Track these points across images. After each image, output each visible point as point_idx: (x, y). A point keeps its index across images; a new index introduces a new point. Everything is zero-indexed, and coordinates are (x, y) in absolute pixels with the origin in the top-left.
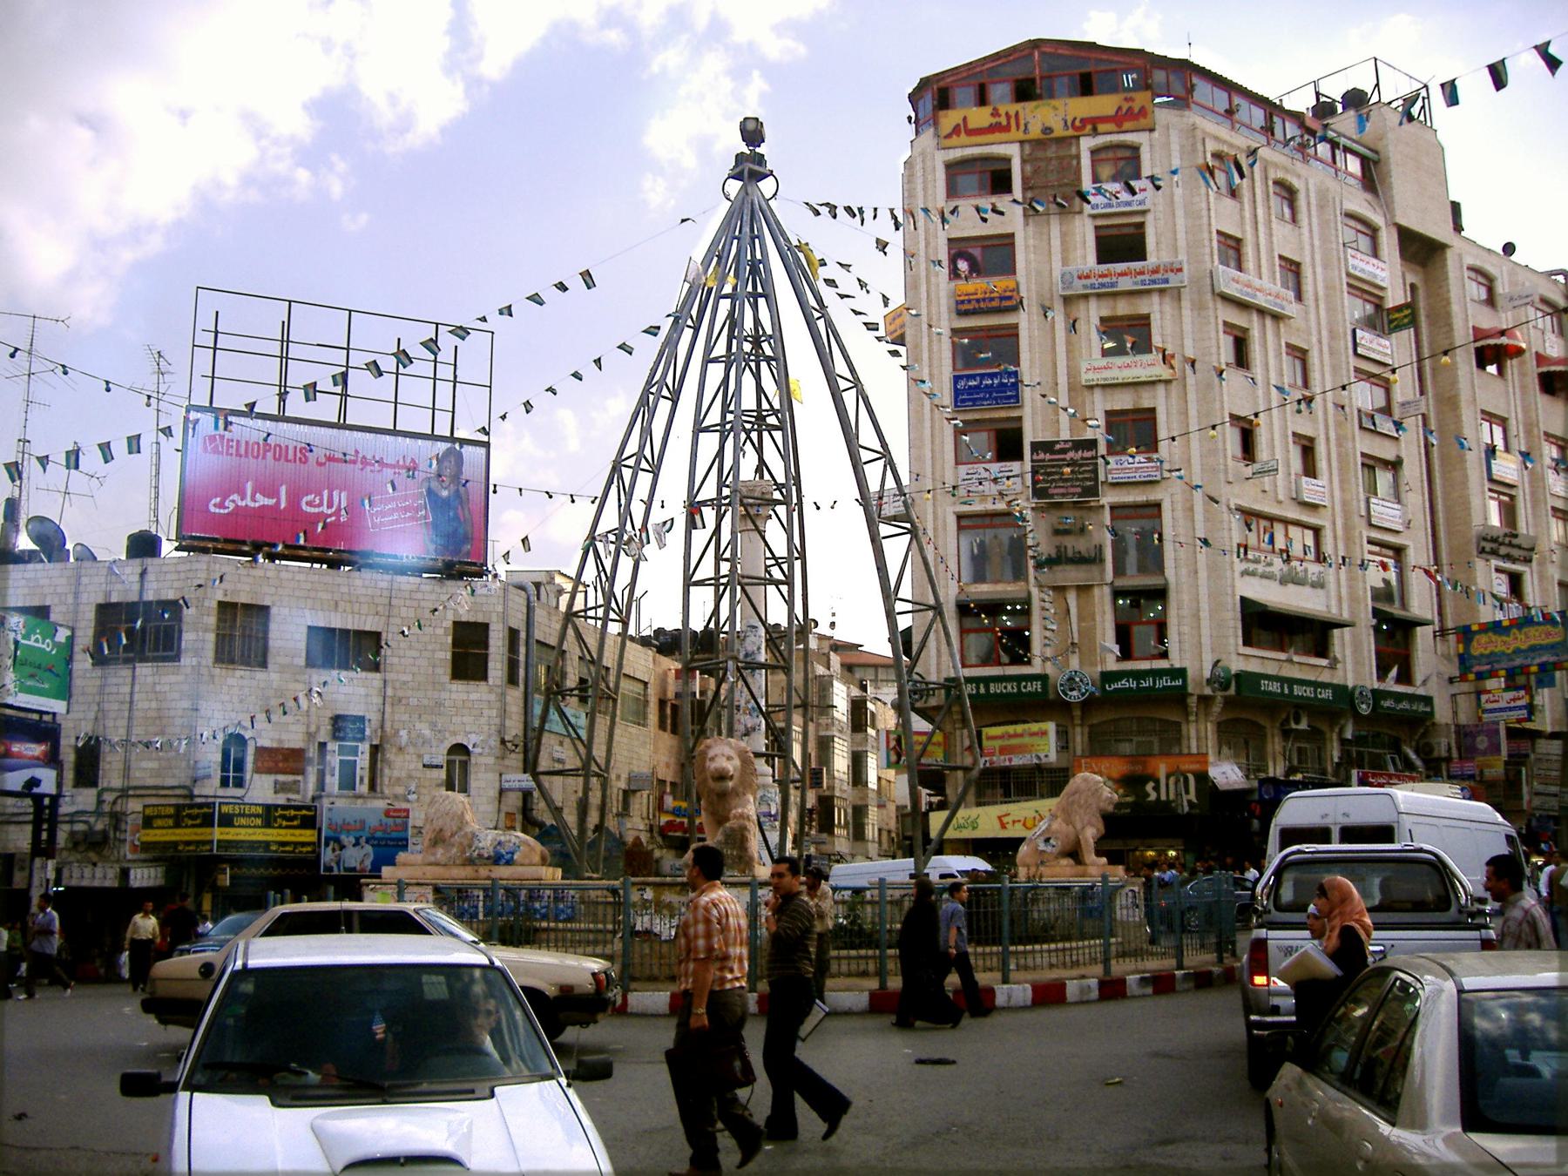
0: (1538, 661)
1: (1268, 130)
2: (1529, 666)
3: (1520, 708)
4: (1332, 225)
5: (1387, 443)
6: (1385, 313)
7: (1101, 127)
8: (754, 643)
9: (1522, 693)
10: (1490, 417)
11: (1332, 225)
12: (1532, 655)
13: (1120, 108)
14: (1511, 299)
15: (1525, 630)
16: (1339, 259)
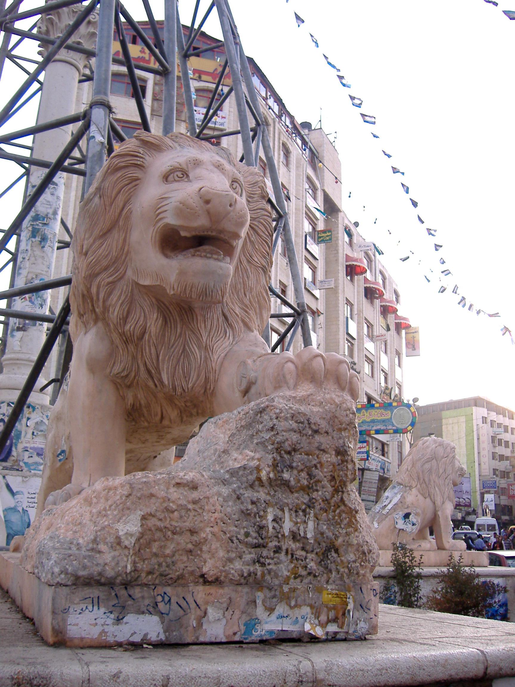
0: (375, 428)
1: (280, 117)
2: (370, 430)
3: (363, 453)
4: (301, 177)
5: (313, 300)
6: (316, 233)
7: (204, 77)
8: (49, 203)
9: (365, 444)
10: (348, 302)
11: (301, 177)
12: (372, 424)
13: (216, 70)
14: (360, 246)
15: (369, 411)
16: (303, 196)
